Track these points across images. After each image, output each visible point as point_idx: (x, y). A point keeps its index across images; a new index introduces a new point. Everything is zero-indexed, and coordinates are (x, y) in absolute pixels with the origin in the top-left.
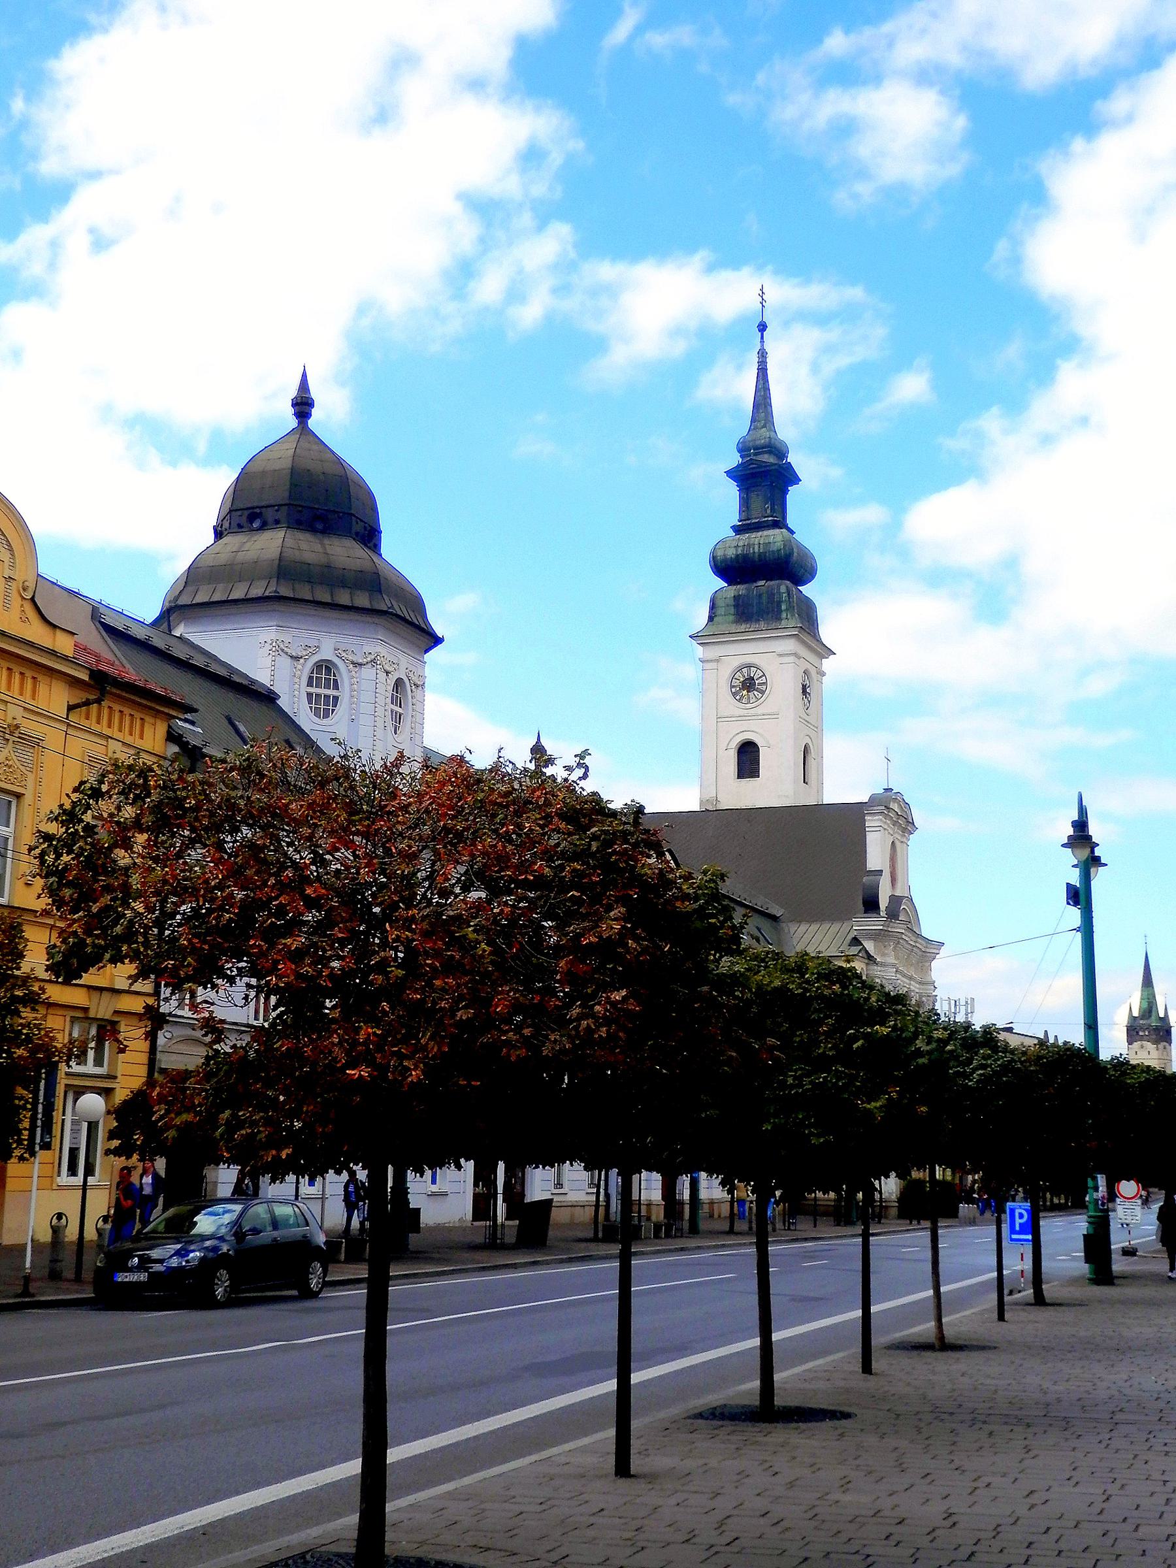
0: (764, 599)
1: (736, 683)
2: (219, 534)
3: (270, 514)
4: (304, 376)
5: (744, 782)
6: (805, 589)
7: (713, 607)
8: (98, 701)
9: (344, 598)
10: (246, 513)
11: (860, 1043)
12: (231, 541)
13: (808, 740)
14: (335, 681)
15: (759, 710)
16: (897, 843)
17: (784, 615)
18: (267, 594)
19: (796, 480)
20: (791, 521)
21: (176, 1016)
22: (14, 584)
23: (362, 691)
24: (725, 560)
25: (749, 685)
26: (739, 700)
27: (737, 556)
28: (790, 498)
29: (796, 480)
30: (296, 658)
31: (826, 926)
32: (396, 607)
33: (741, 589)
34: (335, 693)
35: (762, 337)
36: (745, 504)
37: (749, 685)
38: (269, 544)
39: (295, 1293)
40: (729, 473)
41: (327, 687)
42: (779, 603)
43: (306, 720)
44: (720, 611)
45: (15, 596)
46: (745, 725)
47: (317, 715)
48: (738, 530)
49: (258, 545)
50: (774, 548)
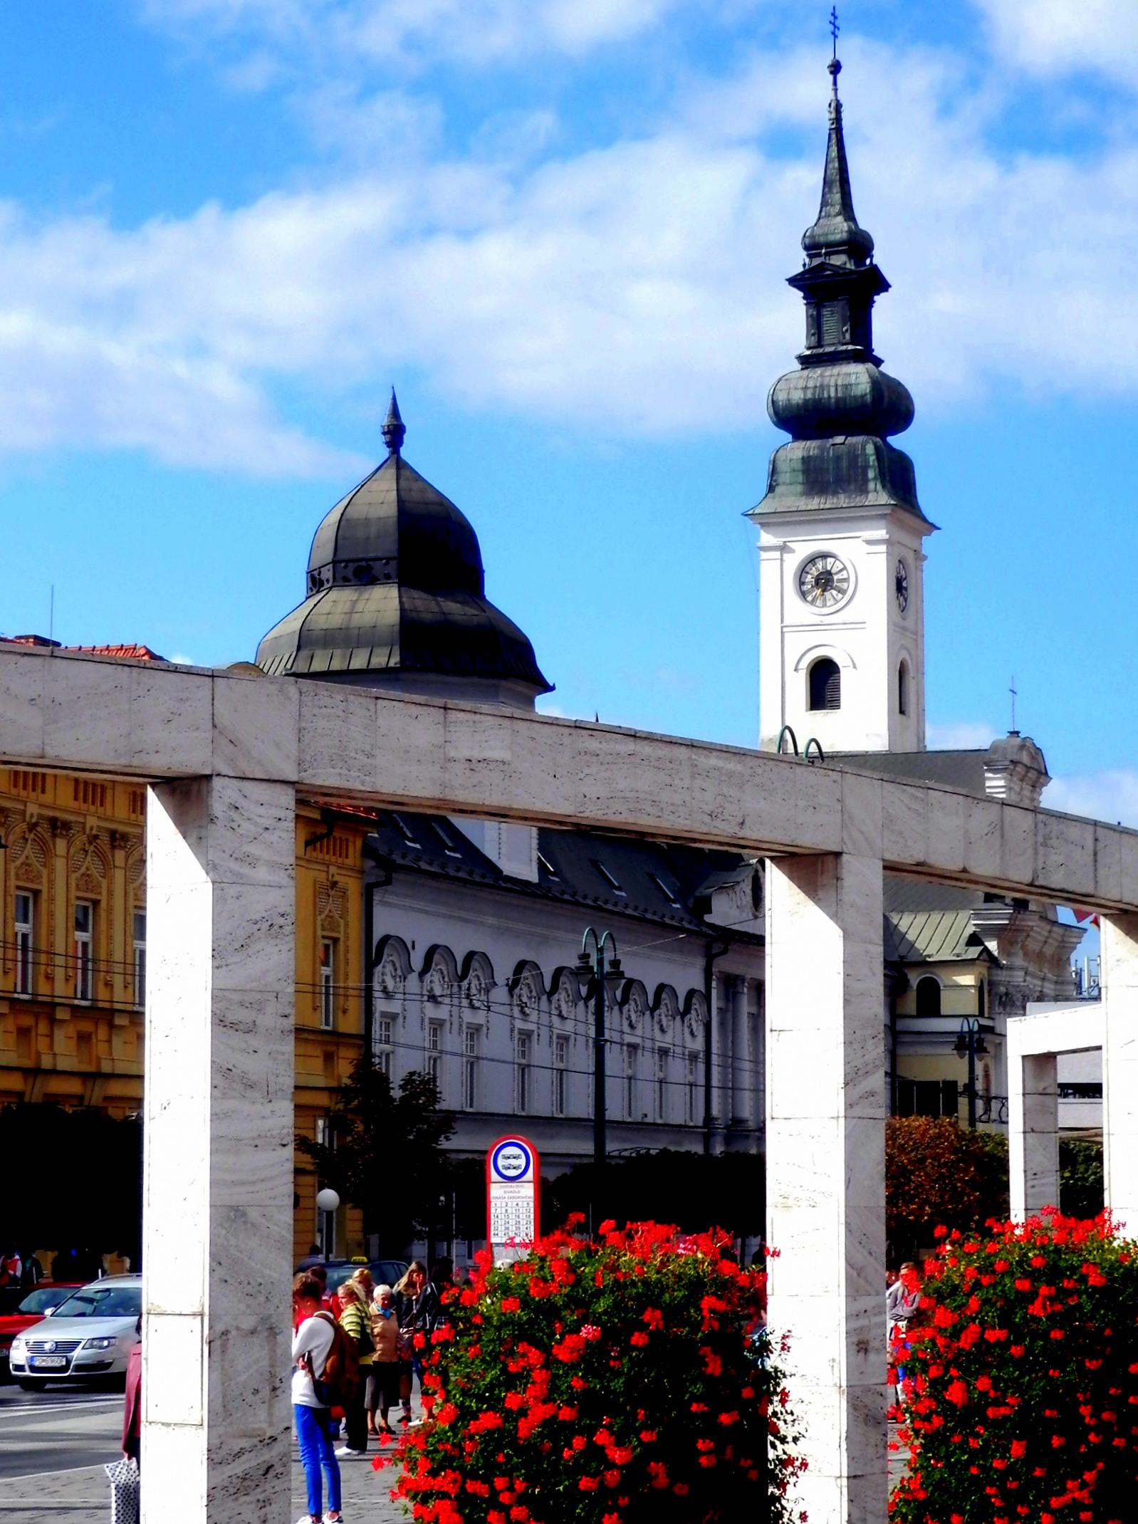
2: (315, 583)
3: (378, 568)
4: (394, 399)
5: (819, 714)
6: (897, 441)
7: (774, 472)
8: (328, 835)
10: (352, 566)
13: (904, 655)
17: (871, 485)
18: (392, 664)
19: (883, 286)
24: (789, 406)
25: (825, 581)
26: (813, 602)
27: (806, 401)
29: (883, 286)
31: (936, 916)
33: (812, 447)
35: (835, 83)
36: (816, 324)
37: (825, 581)
38: (382, 604)
40: (794, 281)
44: (784, 477)
48: (807, 362)
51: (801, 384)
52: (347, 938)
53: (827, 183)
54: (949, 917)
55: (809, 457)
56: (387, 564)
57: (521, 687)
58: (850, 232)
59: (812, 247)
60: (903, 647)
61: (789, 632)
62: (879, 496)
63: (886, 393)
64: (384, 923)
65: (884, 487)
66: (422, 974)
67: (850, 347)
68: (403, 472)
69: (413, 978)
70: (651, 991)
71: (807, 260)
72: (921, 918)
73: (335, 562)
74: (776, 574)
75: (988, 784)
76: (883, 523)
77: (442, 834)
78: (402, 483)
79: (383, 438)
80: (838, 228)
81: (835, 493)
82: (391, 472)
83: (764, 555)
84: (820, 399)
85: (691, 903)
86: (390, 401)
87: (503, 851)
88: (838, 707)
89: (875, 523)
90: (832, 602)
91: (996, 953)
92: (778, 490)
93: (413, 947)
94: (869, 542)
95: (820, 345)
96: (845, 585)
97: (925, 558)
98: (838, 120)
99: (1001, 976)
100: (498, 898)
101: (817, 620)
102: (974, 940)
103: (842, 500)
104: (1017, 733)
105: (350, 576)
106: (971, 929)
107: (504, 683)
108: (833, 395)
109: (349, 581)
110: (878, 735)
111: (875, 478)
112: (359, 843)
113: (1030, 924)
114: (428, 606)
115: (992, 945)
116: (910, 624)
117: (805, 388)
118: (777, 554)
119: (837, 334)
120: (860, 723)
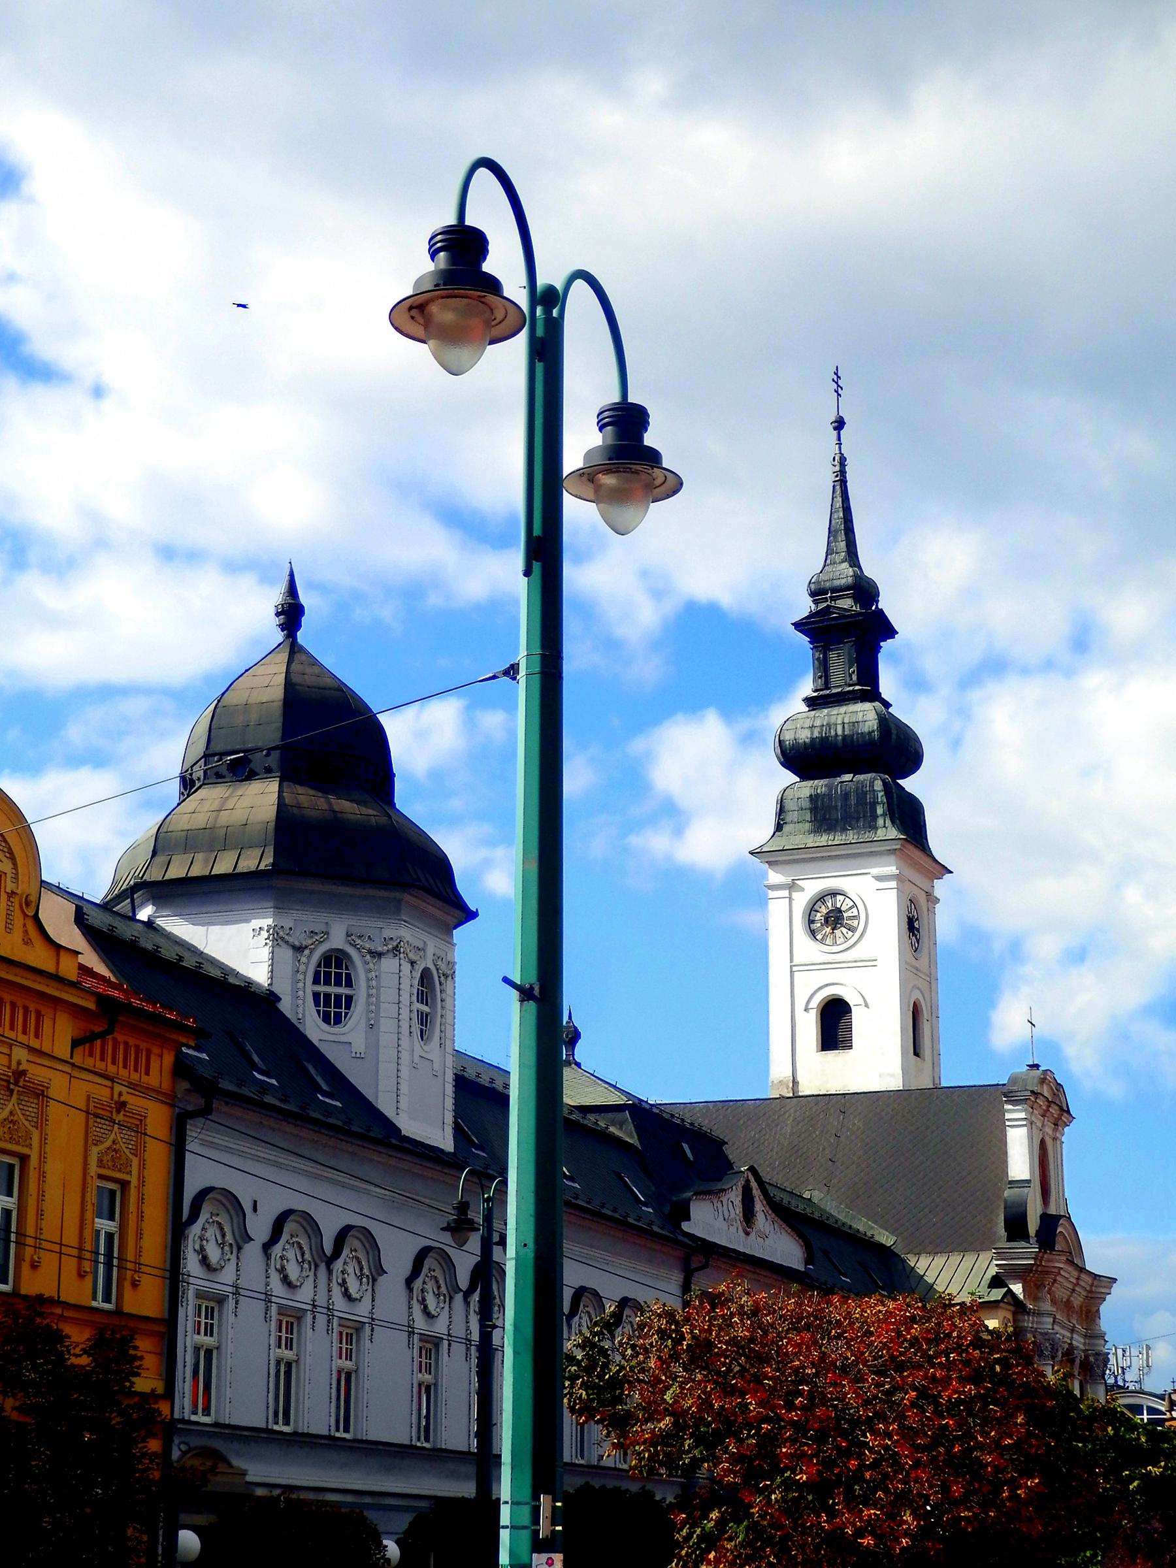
0: (853, 800)
2: (188, 784)
3: (257, 760)
4: (292, 575)
5: (831, 1055)
6: (909, 784)
7: (781, 811)
8: (102, 1036)
11: (1135, 1484)
12: (209, 796)
13: (917, 995)
14: (348, 976)
16: (1049, 1142)
17: (880, 822)
18: (262, 867)
19: (891, 632)
21: (190, 1422)
22: (16, 900)
23: (385, 986)
25: (835, 919)
26: (822, 941)
27: (812, 739)
29: (891, 632)
30: (299, 949)
31: (955, 1258)
32: (423, 880)
34: (347, 991)
36: (823, 670)
37: (835, 919)
38: (259, 800)
41: (338, 984)
42: (874, 804)
43: (315, 1029)
44: (790, 817)
45: (17, 914)
47: (326, 1019)
48: (813, 703)
49: (245, 802)
51: (808, 723)
52: (142, 1180)
53: (831, 532)
54: (969, 1259)
55: (817, 795)
56: (268, 755)
57: (433, 908)
58: (855, 576)
59: (817, 593)
60: (915, 987)
61: (798, 972)
62: (889, 832)
63: (894, 731)
64: (200, 1174)
65: (893, 822)
66: (267, 1247)
67: (857, 688)
68: (297, 656)
69: (253, 1251)
70: (610, 1308)
71: (813, 606)
72: (940, 1260)
73: (207, 756)
74: (782, 917)
75: (1008, 1116)
76: (892, 858)
78: (294, 666)
79: (277, 621)
80: (844, 573)
81: (844, 830)
82: (284, 656)
83: (772, 894)
84: (827, 737)
85: (667, 1209)
86: (287, 578)
87: (401, 1105)
88: (850, 1047)
89: (886, 859)
90: (842, 940)
91: (1021, 1297)
92: (786, 828)
93: (255, 1210)
94: (879, 878)
95: (827, 686)
96: (855, 923)
97: (937, 900)
98: (842, 481)
99: (1028, 1322)
100: (392, 1162)
102: (996, 1282)
103: (851, 836)
104: (1037, 1066)
105: (224, 770)
106: (993, 1271)
107: (407, 897)
108: (840, 732)
109: (223, 777)
110: (892, 1076)
111: (884, 815)
112: (168, 1059)
113: (1057, 1265)
114: (310, 801)
115: (1017, 1288)
116: (923, 963)
117: (812, 727)
118: (786, 893)
119: (843, 675)
120: (876, 1062)
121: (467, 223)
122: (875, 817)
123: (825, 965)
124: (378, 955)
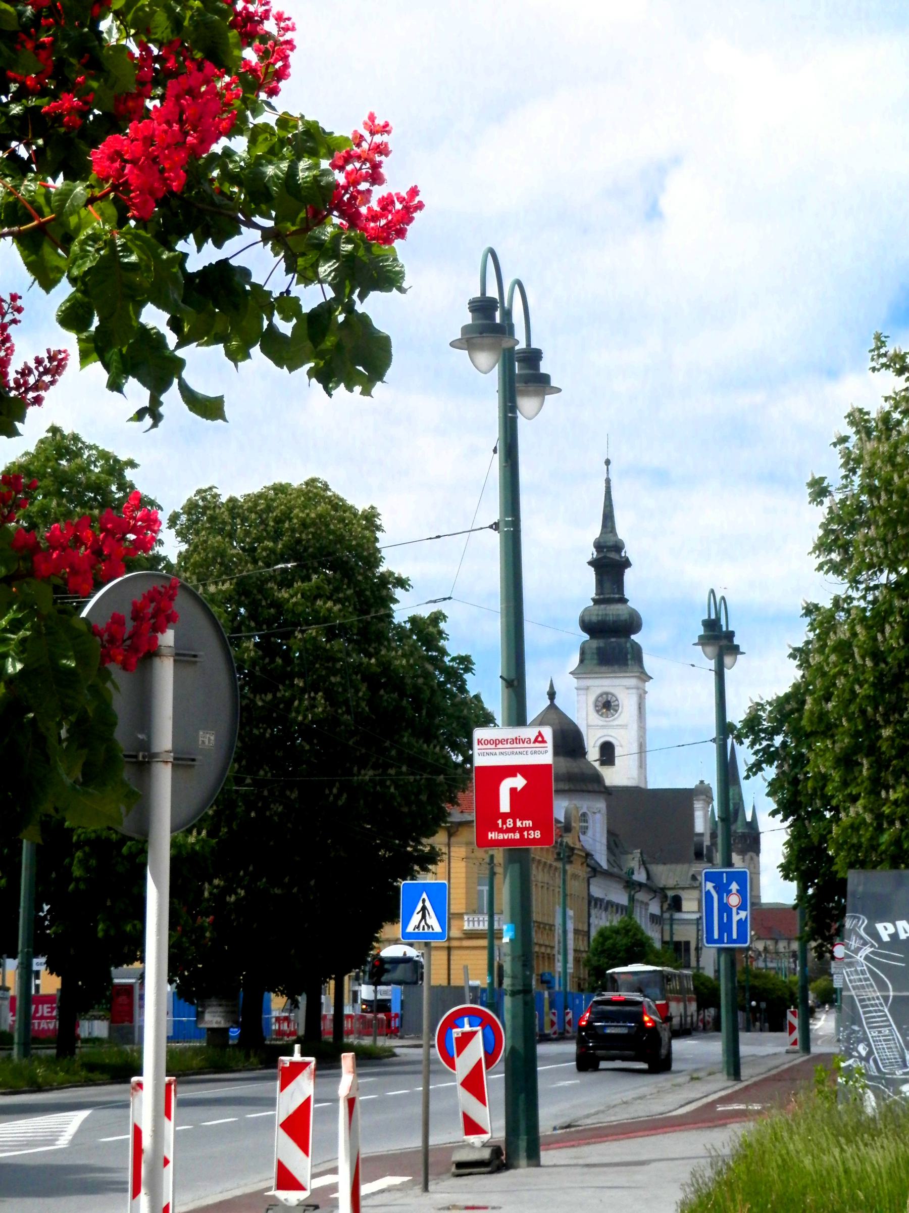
1: (600, 704)
9: (590, 788)
15: (616, 723)
17: (630, 662)
20: (627, 594)
24: (590, 622)
26: (602, 715)
28: (625, 577)
39: (644, 1066)
40: (590, 563)
42: (626, 655)
44: (588, 656)
46: (605, 732)
50: (623, 618)
51: (596, 612)
77: (878, 972)
92: (586, 662)
101: (605, 723)
117: (598, 615)
121: (221, 345)
122: (627, 660)
123: (603, 727)
124: (594, 813)
